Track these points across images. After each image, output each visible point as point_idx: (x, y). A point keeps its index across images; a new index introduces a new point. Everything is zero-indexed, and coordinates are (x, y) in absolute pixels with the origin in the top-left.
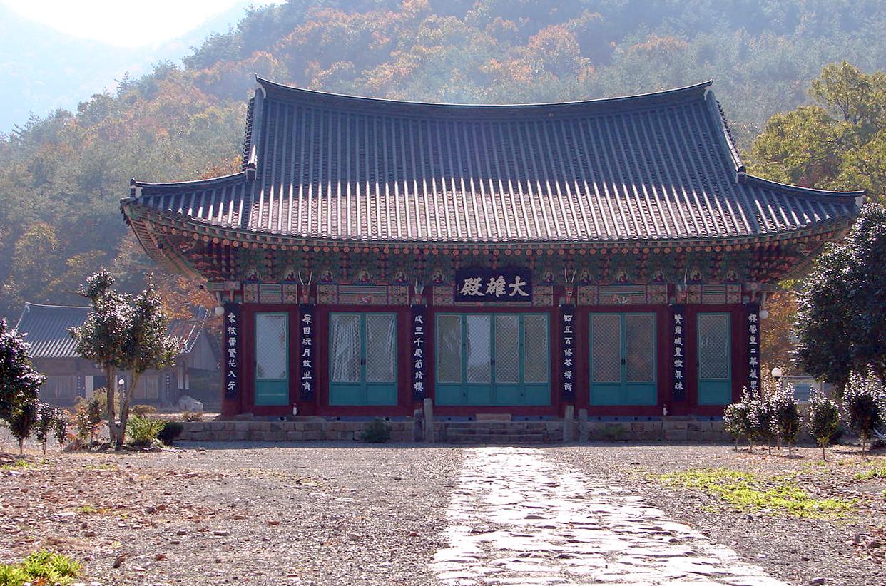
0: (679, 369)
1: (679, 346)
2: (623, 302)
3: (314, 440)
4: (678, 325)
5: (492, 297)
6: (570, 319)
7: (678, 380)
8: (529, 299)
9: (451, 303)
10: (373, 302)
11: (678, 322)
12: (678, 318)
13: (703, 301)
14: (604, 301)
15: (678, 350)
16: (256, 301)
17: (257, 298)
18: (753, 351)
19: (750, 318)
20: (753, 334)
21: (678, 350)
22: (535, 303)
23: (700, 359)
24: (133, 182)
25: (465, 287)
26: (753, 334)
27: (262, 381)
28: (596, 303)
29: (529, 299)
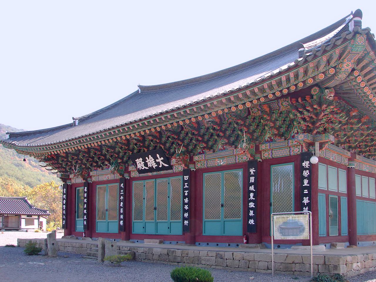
0: (252, 209)
1: (252, 192)
2: (221, 164)
3: (66, 257)
4: (252, 176)
5: (151, 169)
6: (187, 178)
7: (251, 218)
8: (171, 167)
9: (138, 175)
10: (110, 179)
11: (252, 173)
12: (252, 171)
13: (273, 156)
14: (211, 164)
15: (252, 195)
16: (270, 157)
17: (271, 154)
18: (306, 192)
19: (304, 164)
20: (306, 178)
21: (252, 195)
22: (174, 171)
23: (272, 201)
24: (73, 119)
25: (138, 165)
26: (306, 178)
27: (134, 234)
28: (205, 166)
29: (171, 167)
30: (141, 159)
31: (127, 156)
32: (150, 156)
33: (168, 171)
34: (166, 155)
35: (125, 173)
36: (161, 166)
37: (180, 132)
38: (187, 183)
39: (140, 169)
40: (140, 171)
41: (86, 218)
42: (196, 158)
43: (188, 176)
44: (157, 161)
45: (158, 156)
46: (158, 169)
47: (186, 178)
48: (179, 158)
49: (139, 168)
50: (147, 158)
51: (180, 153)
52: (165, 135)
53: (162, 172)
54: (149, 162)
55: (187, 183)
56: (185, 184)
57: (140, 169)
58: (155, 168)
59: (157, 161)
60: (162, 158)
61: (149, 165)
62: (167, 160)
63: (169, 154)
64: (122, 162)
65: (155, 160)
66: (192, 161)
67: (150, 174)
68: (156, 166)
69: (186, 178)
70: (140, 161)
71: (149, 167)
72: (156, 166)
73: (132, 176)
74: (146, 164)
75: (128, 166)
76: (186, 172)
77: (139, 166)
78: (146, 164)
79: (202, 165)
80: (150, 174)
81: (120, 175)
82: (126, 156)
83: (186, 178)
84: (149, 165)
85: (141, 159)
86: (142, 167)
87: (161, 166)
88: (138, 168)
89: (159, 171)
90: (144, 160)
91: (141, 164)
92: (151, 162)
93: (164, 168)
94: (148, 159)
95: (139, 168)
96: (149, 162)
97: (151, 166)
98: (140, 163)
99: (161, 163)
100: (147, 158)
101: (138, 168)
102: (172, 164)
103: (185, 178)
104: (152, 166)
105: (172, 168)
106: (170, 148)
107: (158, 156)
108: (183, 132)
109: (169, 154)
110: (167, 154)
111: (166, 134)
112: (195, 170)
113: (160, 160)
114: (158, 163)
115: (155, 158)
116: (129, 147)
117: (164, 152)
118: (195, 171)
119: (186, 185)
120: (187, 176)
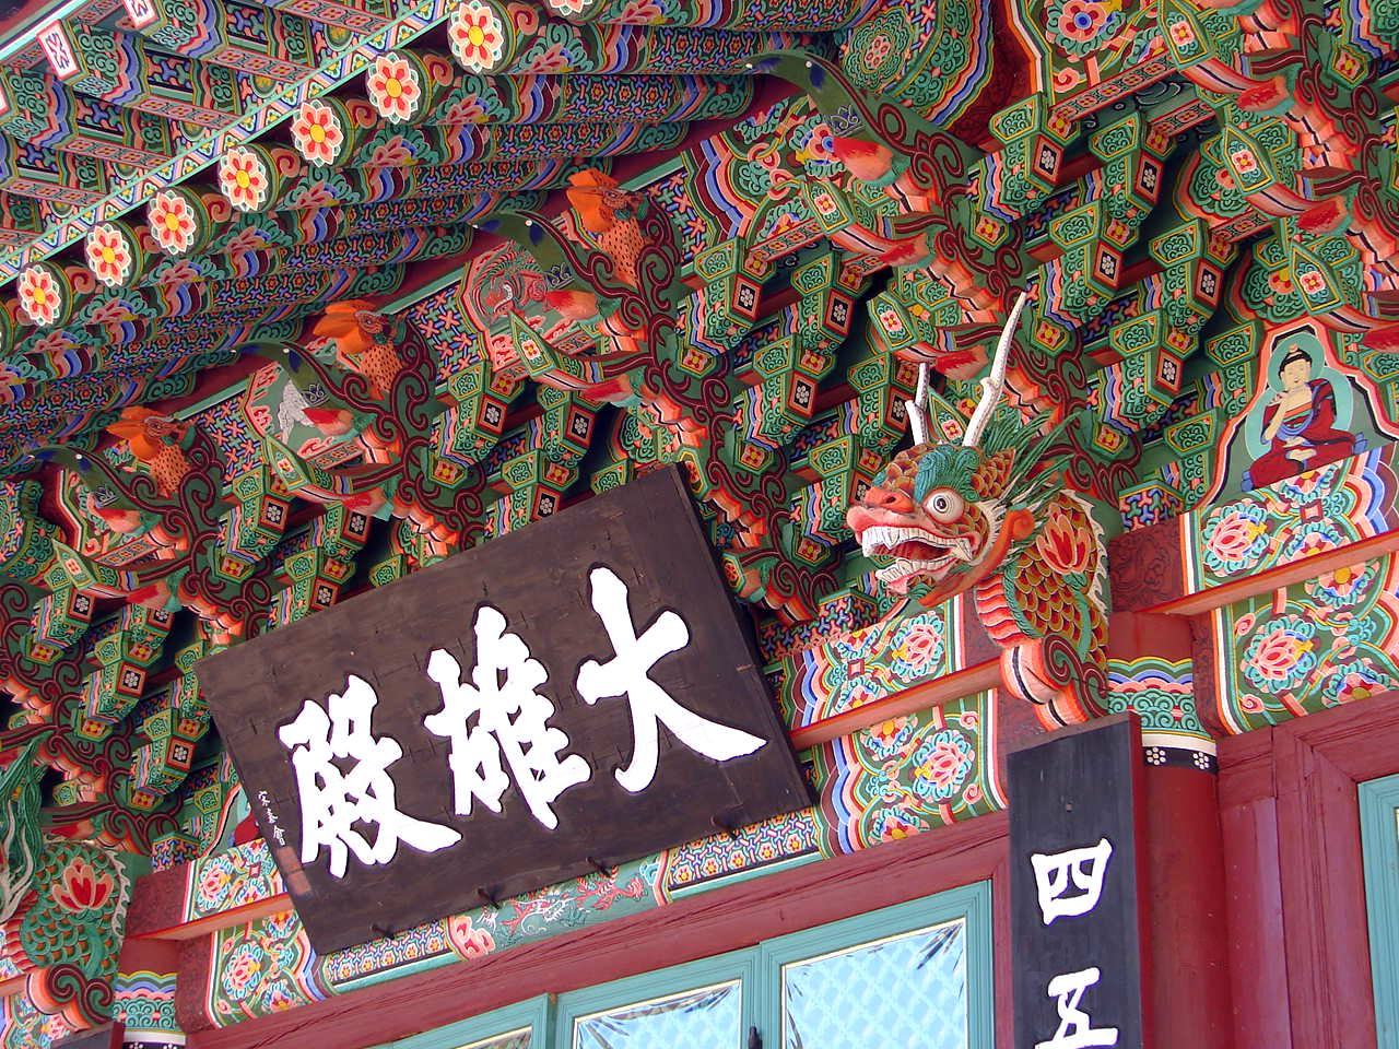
5: (501, 857)
6: (1093, 883)
8: (792, 773)
25: (312, 803)
30: (359, 698)
31: (177, 716)
32: (489, 622)
33: (750, 833)
34: (732, 560)
35: (126, 962)
36: (637, 776)
37: (974, 132)
38: (1091, 976)
39: (338, 868)
40: (344, 906)
41: (1048, 919)
42: (1218, 544)
43: (1101, 853)
44: (594, 683)
45: (608, 594)
46: (602, 829)
47: (1071, 880)
48: (967, 524)
49: (324, 852)
50: (442, 667)
51: (967, 442)
52: (730, 246)
53: (653, 878)
54: (472, 721)
55: (1091, 976)
56: (1060, 986)
57: (338, 868)
58: (549, 820)
59: (594, 683)
60: (670, 633)
61: (475, 782)
62: (744, 658)
63: (768, 564)
64: (110, 811)
65: (559, 689)
66: (1150, 603)
67: (474, 933)
68: (577, 771)
69: (1071, 880)
70: (341, 729)
71: (463, 807)
72: (577, 771)
73: (216, 1010)
74: (423, 780)
75: (188, 851)
76: (1053, 784)
77: (326, 824)
78: (423, 780)
79: (1341, 639)
80: (477, 935)
81: (52, 987)
82: (158, 726)
83: (1072, 891)
84: (475, 782)
85: (359, 698)
86: (369, 831)
87: (637, 776)
88: (309, 854)
89: (604, 870)
90: (405, 713)
91: (355, 782)
92: (500, 724)
93: (695, 800)
94: (466, 678)
95: (324, 852)
96: (472, 721)
97: (491, 793)
98: (345, 765)
99: (652, 707)
100: (442, 667)
101: (309, 854)
102: (815, 707)
103: (1046, 892)
104: (514, 796)
105: (820, 777)
106: (787, 464)
107: (608, 594)
108: (1015, 124)
109: (768, 564)
110: (748, 559)
111: (740, 225)
112: (1202, 746)
113: (632, 663)
114: (598, 731)
115: (564, 641)
116: (203, 538)
117: (705, 520)
118: (1202, 763)
119: (1069, 1014)
120: (1077, 856)
